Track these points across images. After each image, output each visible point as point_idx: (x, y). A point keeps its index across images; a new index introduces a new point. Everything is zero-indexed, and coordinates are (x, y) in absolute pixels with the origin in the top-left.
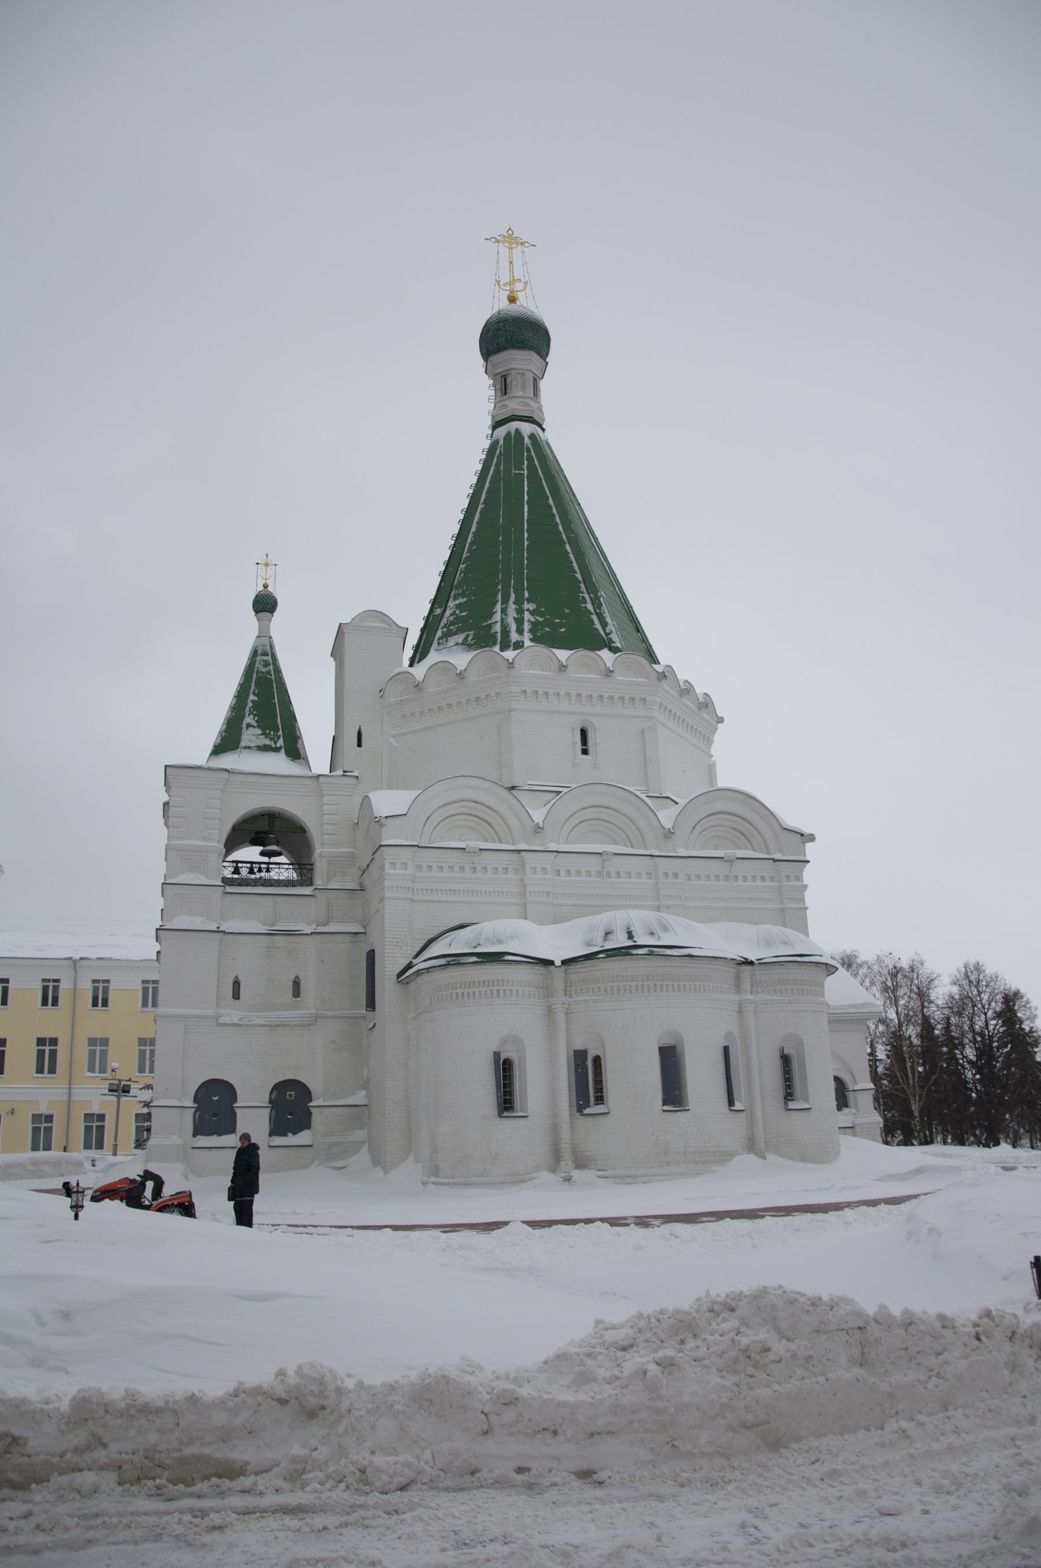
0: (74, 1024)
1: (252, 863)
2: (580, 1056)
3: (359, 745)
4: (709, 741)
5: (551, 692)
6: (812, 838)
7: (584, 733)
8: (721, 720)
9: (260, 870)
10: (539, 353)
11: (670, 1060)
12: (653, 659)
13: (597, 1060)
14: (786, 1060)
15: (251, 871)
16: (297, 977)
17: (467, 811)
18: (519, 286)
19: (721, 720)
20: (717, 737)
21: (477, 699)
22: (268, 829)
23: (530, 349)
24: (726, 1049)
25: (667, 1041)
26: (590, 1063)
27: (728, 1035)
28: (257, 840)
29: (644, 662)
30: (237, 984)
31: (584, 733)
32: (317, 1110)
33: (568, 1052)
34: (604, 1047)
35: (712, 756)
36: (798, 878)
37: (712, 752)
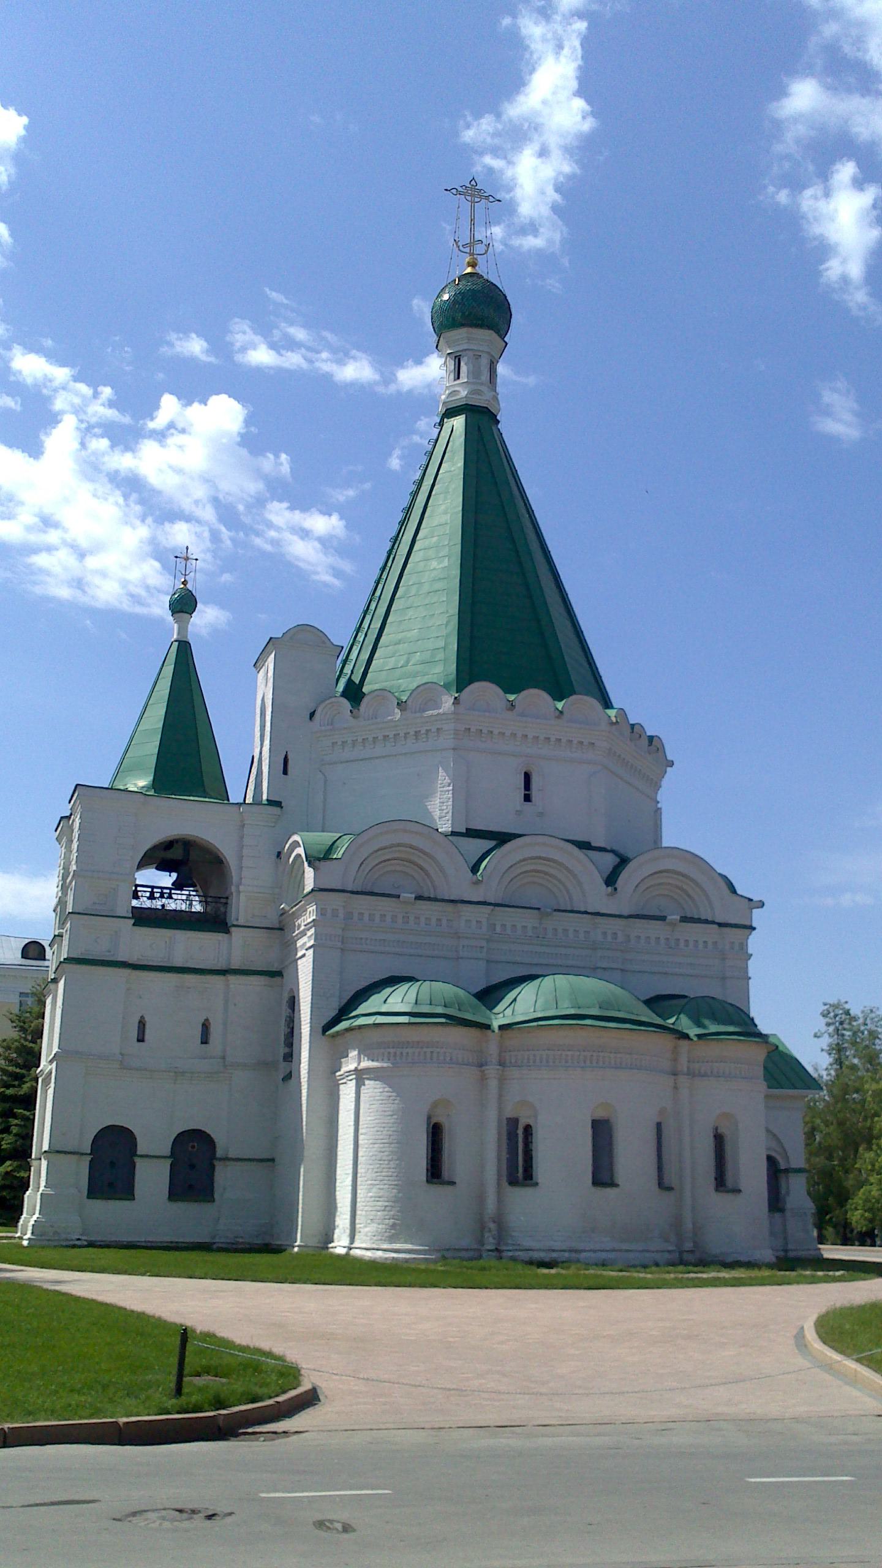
0: (476, 1151)
1: (153, 887)
2: (513, 1122)
3: (285, 772)
4: (657, 786)
5: (496, 732)
6: (762, 904)
7: (527, 777)
8: (671, 764)
9: (162, 896)
10: (498, 332)
11: (602, 1132)
12: (607, 704)
13: (528, 1129)
14: (719, 1140)
15: (152, 897)
16: (207, 1020)
17: (403, 856)
18: (479, 249)
19: (671, 764)
20: (665, 782)
21: (417, 733)
22: (182, 858)
23: (489, 328)
24: (659, 1125)
25: (600, 1114)
26: (520, 1132)
27: (662, 1112)
28: (165, 866)
29: (598, 706)
30: (142, 1024)
31: (527, 777)
32: (221, 1163)
33: (499, 1121)
34: (536, 1117)
35: (498, 422)
36: (743, 946)
37: (659, 799)
